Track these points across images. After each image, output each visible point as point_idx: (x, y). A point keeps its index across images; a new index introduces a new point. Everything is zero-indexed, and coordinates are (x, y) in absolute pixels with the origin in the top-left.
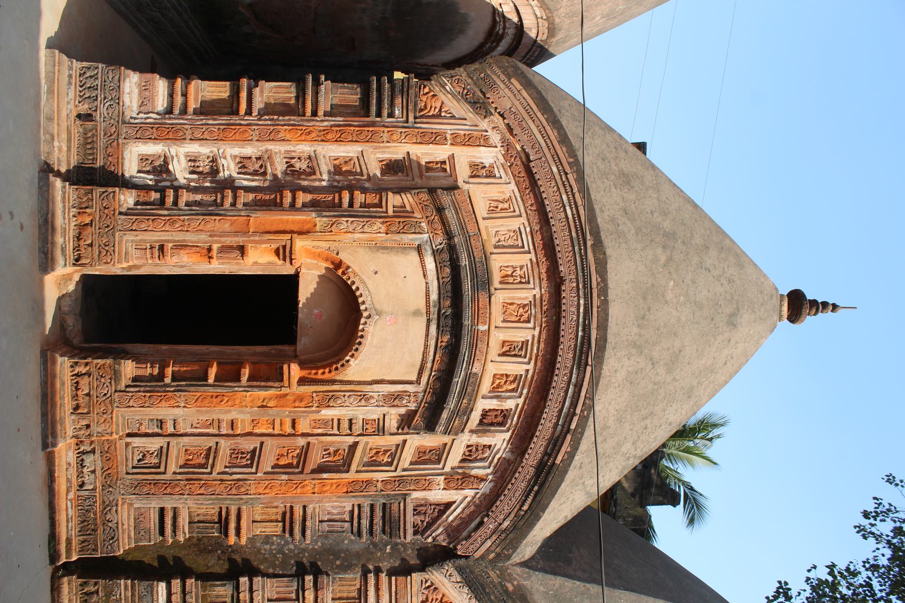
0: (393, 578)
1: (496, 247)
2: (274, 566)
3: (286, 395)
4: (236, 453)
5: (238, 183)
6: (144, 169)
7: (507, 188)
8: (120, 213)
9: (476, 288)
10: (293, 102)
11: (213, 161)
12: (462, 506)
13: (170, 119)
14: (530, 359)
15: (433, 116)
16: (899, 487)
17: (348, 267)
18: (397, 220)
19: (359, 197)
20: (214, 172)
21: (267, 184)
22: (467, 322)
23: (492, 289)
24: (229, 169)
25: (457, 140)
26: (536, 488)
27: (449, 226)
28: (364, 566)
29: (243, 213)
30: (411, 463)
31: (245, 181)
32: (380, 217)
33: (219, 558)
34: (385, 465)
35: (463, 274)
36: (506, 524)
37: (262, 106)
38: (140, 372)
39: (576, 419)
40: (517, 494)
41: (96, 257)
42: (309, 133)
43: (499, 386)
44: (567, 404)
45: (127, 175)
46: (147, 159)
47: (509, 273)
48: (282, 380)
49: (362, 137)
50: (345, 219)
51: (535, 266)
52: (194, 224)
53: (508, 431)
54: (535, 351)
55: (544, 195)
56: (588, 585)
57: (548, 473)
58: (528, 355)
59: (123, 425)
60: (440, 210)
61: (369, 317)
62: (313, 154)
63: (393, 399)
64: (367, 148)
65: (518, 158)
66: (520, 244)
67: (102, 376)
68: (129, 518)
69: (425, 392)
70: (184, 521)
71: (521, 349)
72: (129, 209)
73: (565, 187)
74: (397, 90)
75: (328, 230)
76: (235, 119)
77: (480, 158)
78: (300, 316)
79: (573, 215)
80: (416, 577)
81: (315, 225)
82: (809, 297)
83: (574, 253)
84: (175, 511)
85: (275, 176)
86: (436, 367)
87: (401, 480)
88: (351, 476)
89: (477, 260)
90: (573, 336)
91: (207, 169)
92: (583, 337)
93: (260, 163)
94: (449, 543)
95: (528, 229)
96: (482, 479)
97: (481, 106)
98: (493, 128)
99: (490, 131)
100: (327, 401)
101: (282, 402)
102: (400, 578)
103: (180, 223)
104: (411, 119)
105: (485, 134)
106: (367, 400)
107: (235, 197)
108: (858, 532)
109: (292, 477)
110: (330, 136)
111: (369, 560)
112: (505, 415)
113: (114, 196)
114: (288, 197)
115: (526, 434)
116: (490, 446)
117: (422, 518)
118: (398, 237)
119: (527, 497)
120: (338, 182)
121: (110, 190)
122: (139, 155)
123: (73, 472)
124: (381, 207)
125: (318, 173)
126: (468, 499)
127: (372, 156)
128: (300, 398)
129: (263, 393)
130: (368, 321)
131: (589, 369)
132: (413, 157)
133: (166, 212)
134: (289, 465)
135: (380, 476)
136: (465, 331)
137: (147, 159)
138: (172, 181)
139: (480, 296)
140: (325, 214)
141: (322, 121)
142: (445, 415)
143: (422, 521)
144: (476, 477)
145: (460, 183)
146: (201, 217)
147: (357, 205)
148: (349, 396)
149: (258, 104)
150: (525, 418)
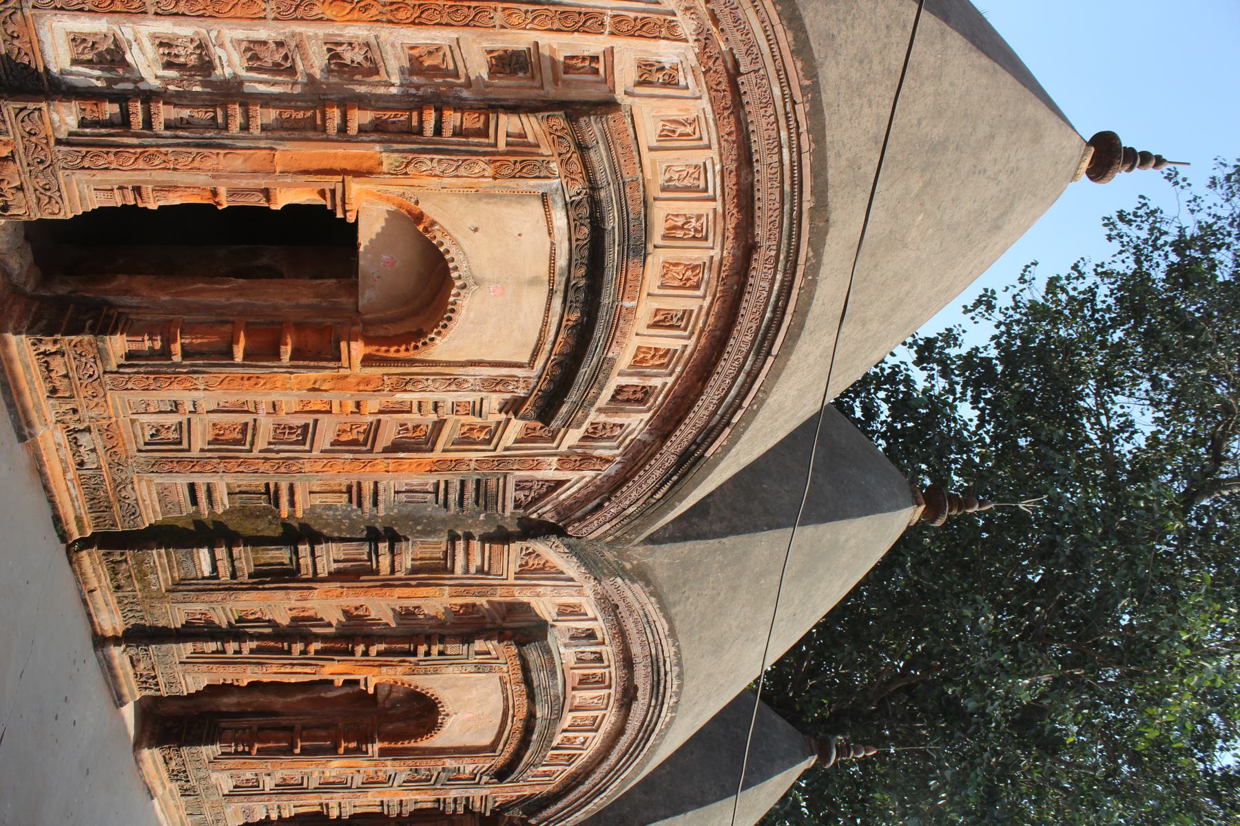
0: (487, 546)
2: (340, 530)
3: (346, 377)
4: (282, 430)
5: (249, 88)
6: (82, 57)
7: (696, 105)
8: (59, 142)
9: (625, 255)
11: (200, 46)
12: (578, 485)
14: (692, 333)
16: (1178, 187)
17: (433, 223)
18: (512, 159)
19: (452, 119)
20: (206, 66)
21: (298, 90)
22: (606, 300)
23: (650, 247)
24: (229, 63)
26: (675, 478)
27: (594, 174)
28: (450, 531)
29: (262, 144)
30: (516, 441)
31: (260, 85)
32: (485, 154)
33: (271, 523)
34: (481, 443)
35: (608, 240)
36: (631, 510)
38: (134, 347)
39: (740, 413)
40: (649, 482)
41: (34, 206)
43: (644, 360)
44: (733, 392)
45: (54, 70)
46: (84, 40)
47: (680, 224)
48: (339, 359)
50: (429, 157)
51: (720, 219)
52: (183, 160)
53: (649, 410)
54: (700, 324)
55: (751, 128)
56: (723, 540)
57: (694, 464)
58: (690, 328)
59: (124, 407)
60: (582, 148)
61: (464, 287)
62: (373, 41)
63: (494, 384)
64: (466, 35)
65: (719, 62)
66: (702, 185)
67: (80, 355)
68: (150, 494)
69: (540, 377)
70: (221, 494)
71: (681, 319)
72: (71, 134)
73: (788, 121)
75: (400, 172)
77: (656, 54)
78: (361, 262)
79: (791, 162)
80: (516, 547)
81: (381, 164)
82: (1126, 142)
83: (782, 212)
86: (557, 349)
87: (501, 460)
88: (437, 455)
89: (631, 216)
90: (757, 316)
92: (771, 320)
93: (283, 51)
94: (559, 521)
95: (718, 167)
96: (607, 461)
98: (687, 9)
99: (679, 13)
100: (404, 384)
101: (341, 384)
102: (495, 546)
103: (163, 158)
105: (670, 18)
106: (459, 385)
107: (247, 116)
108: (1105, 225)
109: (358, 456)
110: (401, 15)
111: (457, 526)
112: (647, 392)
113: (41, 117)
114: (335, 115)
115: (672, 416)
116: (621, 426)
117: (527, 493)
118: (512, 183)
119: (662, 485)
120: (418, 87)
121: (31, 106)
122: (68, 34)
123: (67, 453)
124: (487, 136)
125: (382, 71)
126: (587, 479)
127: (475, 46)
129: (313, 375)
130: (463, 292)
131: (770, 360)
132: (545, 51)
133: (135, 141)
134: (354, 442)
135: (474, 456)
136: (602, 313)
137: (84, 40)
138: (135, 82)
139: (630, 264)
140: (396, 146)
142: (564, 409)
143: (526, 496)
144: (601, 459)
145: (619, 96)
146: (195, 150)
147: (447, 132)
148: (434, 380)
150: (673, 398)
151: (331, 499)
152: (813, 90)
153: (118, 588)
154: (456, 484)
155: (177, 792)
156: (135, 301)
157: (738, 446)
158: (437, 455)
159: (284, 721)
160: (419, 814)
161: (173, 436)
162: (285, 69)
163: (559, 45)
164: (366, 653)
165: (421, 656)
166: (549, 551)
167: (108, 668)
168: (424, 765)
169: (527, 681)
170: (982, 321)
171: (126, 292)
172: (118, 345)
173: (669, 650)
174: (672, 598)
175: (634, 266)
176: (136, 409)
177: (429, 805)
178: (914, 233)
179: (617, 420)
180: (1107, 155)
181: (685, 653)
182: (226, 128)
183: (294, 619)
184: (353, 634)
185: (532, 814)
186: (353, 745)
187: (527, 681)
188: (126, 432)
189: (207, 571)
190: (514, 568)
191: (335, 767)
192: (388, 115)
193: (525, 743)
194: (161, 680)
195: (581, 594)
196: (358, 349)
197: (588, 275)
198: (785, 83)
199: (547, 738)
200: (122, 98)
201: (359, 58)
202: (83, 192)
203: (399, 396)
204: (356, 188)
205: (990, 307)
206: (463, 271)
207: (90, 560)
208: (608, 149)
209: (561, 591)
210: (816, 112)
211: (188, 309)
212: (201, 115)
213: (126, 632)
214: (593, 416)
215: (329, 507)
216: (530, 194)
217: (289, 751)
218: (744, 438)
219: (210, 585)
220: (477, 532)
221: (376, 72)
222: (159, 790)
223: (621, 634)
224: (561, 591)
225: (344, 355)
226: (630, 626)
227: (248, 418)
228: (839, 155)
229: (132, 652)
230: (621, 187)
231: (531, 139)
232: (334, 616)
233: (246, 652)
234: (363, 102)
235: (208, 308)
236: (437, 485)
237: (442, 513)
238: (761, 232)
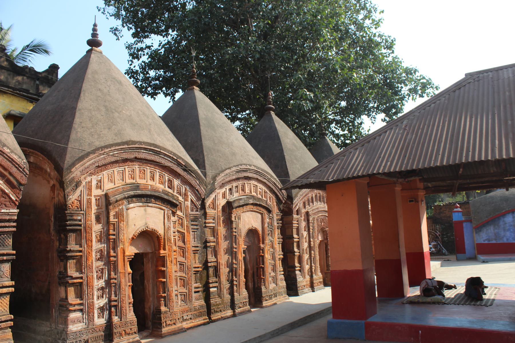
0: (15, 224)
1: (123, 181)
4: (181, 270)
5: (107, 279)
8: (121, 320)
10: (75, 261)
13: (85, 309)
15: (80, 203)
19: (111, 232)
20: (102, 288)
21: (106, 267)
22: (149, 193)
25: (90, 194)
37: (78, 273)
38: (163, 305)
42: (89, 253)
45: (105, 322)
49: (90, 231)
52: (123, 292)
60: (117, 201)
63: (169, 218)
64: (93, 230)
74: (71, 218)
76: (85, 283)
80: (207, 211)
84: (196, 288)
85: (104, 265)
87: (186, 216)
88: (185, 232)
91: (101, 291)
96: (186, 189)
97: (78, 184)
100: (169, 240)
104: (82, 212)
107: (113, 279)
110: (90, 245)
114: (112, 259)
118: (125, 217)
120: (104, 240)
128: (169, 249)
129: (168, 262)
131: (162, 151)
134: (183, 252)
141: (84, 248)
142: (174, 201)
145: (104, 193)
147: (114, 233)
149: (77, 275)
151: (197, 258)
153: (221, 311)
154: (192, 227)
155: (276, 298)
156: (152, 306)
157: (182, 157)
158: (185, 232)
159: (255, 270)
160: (282, 233)
161: (183, 297)
162: (102, 271)
163: (94, 208)
164: (236, 248)
165: (236, 234)
166: (209, 202)
167: (241, 313)
168: (267, 232)
169: (243, 206)
170: (122, 33)
171: (150, 308)
172: (163, 308)
173: (234, 169)
174: (220, 169)
175: (141, 187)
176: (178, 304)
177: (279, 231)
178: (128, 113)
179: (176, 187)
180: (94, 43)
181: (235, 164)
182: (116, 283)
183: (227, 267)
184: (231, 252)
185: (282, 202)
186: (261, 251)
187: (243, 206)
188: (183, 308)
189: (216, 289)
190: (213, 211)
191: (268, 256)
192: (111, 247)
193: (260, 205)
194: (244, 301)
195: (219, 193)
196: (162, 252)
197: (144, 198)
199: (259, 199)
200: (110, 307)
201: (99, 254)
202: (131, 316)
203: (172, 242)
204: (127, 253)
205: (116, 29)
206: (144, 227)
207: (214, 317)
208: (116, 195)
209: (219, 198)
210: (106, 147)
211: (154, 293)
212: (113, 289)
213: (232, 309)
214: (175, 194)
215: (199, 258)
216: (127, 213)
217: (263, 268)
218: (180, 155)
219: (219, 288)
220: (204, 221)
221: (101, 250)
222: (275, 302)
223: (230, 181)
224: (219, 198)
225: (163, 255)
226: (228, 180)
227: (178, 278)
228: (115, 139)
229: (237, 308)
231: (115, 213)
232: (227, 256)
233: (236, 279)
234: (108, 252)
235: (153, 288)
236: (193, 231)
237: (199, 230)
238: (132, 156)
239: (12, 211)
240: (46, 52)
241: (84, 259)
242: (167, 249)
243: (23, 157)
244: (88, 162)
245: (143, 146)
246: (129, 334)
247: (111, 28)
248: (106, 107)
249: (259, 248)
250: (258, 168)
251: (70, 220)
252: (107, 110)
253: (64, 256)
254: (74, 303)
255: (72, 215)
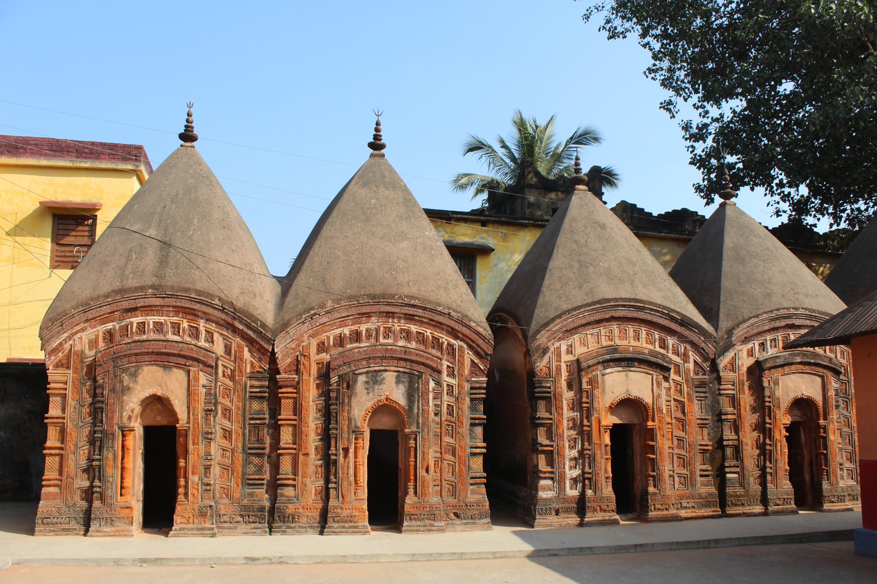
0: (484, 391)
4: (679, 447)
19: (584, 399)
20: (575, 459)
22: (630, 356)
60: (589, 367)
63: (659, 384)
64: (564, 397)
75: (599, 412)
76: (555, 451)
80: (721, 374)
84: (701, 470)
87: (687, 381)
88: (686, 400)
96: (685, 348)
97: (545, 351)
100: (660, 410)
114: (585, 428)
123: (688, 511)
128: (660, 421)
129: (658, 436)
145: (575, 358)
149: (547, 442)
152: (569, 311)
154: (697, 394)
158: (686, 400)
159: (814, 457)
163: (564, 374)
164: (770, 424)
166: (723, 362)
169: (782, 366)
170: (678, 107)
172: (651, 489)
173: (765, 316)
174: (741, 319)
179: (671, 347)
181: (767, 310)
184: (762, 428)
186: (822, 430)
187: (782, 366)
190: (732, 374)
194: (786, 497)
195: (741, 350)
196: (650, 423)
198: (568, 318)
200: (584, 479)
202: (608, 491)
203: (664, 411)
204: (603, 423)
205: (670, 103)
207: (730, 511)
210: (574, 309)
212: (587, 461)
215: (709, 434)
217: (826, 455)
218: (673, 307)
219: (742, 475)
220: (717, 387)
223: (760, 333)
227: (675, 456)
230: (598, 356)
232: (755, 434)
234: (582, 421)
239: (481, 379)
240: (596, 139)
241: (554, 427)
242: (656, 420)
243: (488, 328)
244: (555, 327)
245: (621, 303)
246: (605, 511)
247: (661, 103)
248: (579, 261)
249: (819, 426)
250: (814, 311)
251: (539, 387)
252: (581, 265)
253: (535, 424)
254: (544, 470)
255: (540, 382)
